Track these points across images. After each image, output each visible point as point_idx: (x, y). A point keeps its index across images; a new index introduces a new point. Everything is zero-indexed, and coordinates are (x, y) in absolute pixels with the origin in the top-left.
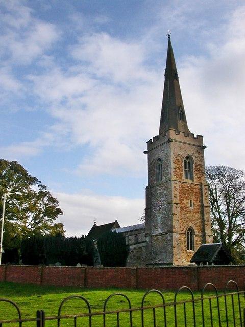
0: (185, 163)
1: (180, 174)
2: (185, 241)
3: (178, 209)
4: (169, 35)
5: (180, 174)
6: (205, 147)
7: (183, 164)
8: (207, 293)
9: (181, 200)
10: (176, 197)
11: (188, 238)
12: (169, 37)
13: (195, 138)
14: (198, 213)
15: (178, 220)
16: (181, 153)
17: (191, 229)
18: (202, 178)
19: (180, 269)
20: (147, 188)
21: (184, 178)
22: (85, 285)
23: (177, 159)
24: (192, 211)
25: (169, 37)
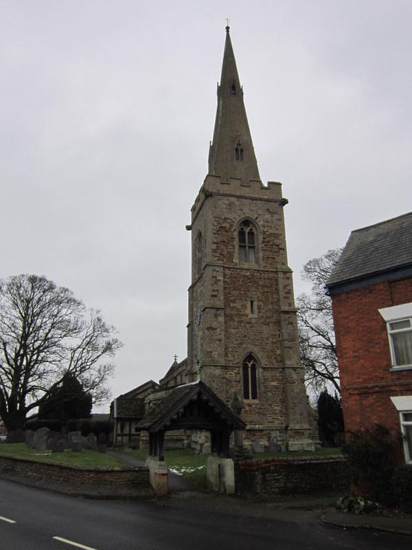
0: (242, 233)
1: (229, 253)
2: (239, 382)
3: (221, 319)
4: (228, 28)
5: (229, 253)
6: (285, 202)
7: (236, 234)
8: (101, 422)
9: (227, 300)
10: (215, 296)
11: (246, 375)
12: (228, 31)
13: (266, 188)
14: (268, 324)
15: (220, 340)
16: (230, 216)
17: (250, 357)
18: (277, 259)
19: (39, 411)
20: (121, 396)
21: (236, 260)
22: (392, 299)
23: (221, 227)
24: (253, 321)
25: (228, 31)
